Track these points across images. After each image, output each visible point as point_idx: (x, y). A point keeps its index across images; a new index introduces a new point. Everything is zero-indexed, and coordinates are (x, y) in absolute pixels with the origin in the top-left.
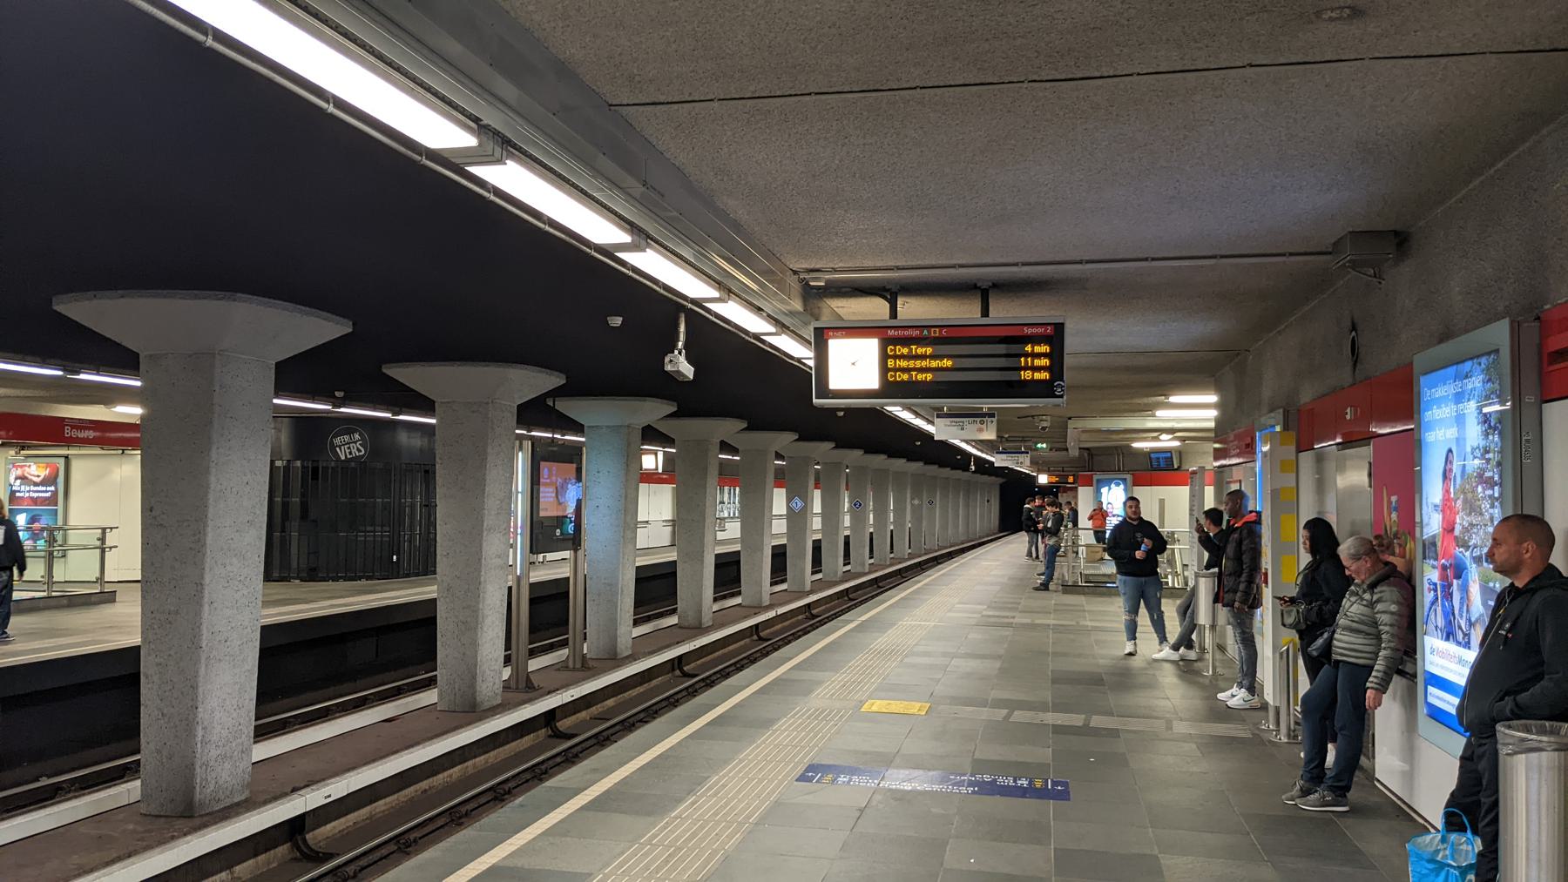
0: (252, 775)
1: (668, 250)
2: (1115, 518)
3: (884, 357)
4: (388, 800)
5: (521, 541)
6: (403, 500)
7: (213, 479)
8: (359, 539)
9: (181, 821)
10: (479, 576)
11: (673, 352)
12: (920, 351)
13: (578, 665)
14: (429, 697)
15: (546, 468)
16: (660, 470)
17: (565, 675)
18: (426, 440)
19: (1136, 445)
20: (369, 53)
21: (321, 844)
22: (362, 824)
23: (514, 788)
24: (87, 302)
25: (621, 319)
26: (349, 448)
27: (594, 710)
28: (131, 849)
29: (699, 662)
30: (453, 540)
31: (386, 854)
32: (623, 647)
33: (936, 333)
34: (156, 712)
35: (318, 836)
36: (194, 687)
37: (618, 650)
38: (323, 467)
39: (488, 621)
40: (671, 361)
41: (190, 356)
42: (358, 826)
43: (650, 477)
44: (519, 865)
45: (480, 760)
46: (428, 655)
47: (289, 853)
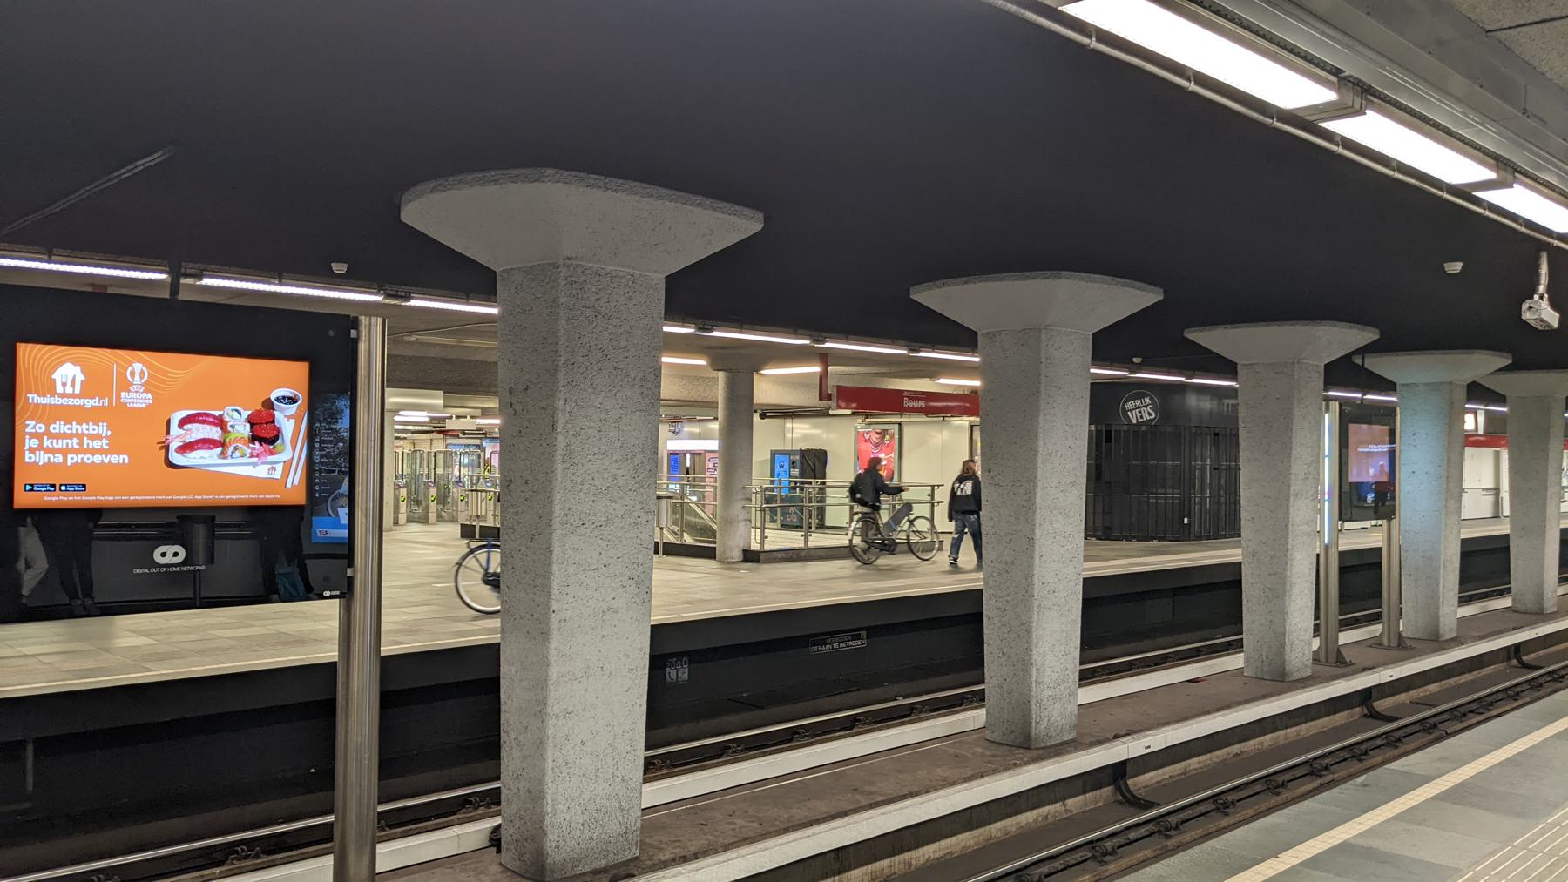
0: (1079, 715)
1: (1539, 183)
4: (1202, 758)
5: (1328, 507)
6: (1193, 463)
7: (1041, 443)
8: (1151, 500)
9: (1022, 751)
10: (1287, 543)
11: (1532, 298)
13: (1394, 643)
14: (1235, 661)
15: (1358, 431)
16: (1481, 431)
17: (1377, 654)
18: (1215, 403)
20: (1237, 24)
21: (1141, 791)
22: (1177, 778)
23: (1332, 765)
24: (937, 290)
25: (1461, 264)
26: (1141, 412)
27: (1416, 694)
28: (983, 769)
29: (1541, 653)
30: (1258, 505)
31: (1204, 811)
32: (1447, 629)
35: (1140, 783)
36: (1029, 631)
37: (1441, 632)
38: (1115, 431)
39: (1296, 591)
40: (1530, 308)
41: (1020, 332)
42: (1174, 780)
43: (1472, 440)
44: (1375, 847)
45: (1291, 732)
46: (1234, 619)
47: (1113, 796)
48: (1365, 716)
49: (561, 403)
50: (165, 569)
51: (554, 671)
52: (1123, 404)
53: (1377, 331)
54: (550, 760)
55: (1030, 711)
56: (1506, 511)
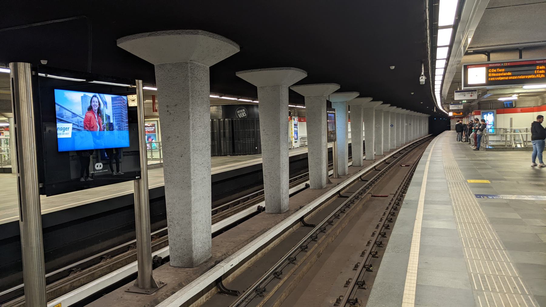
2: (489, 126)
3: (488, 73)
12: (500, 70)
13: (337, 177)
19: (500, 99)
22: (311, 218)
26: (242, 114)
33: (506, 64)
34: (269, 185)
36: (279, 178)
40: (422, 78)
41: (273, 86)
48: (338, 197)
49: (191, 109)
50: (98, 171)
51: (193, 199)
52: (237, 112)
53: (340, 85)
54: (193, 228)
55: (281, 202)
56: (162, 157)
